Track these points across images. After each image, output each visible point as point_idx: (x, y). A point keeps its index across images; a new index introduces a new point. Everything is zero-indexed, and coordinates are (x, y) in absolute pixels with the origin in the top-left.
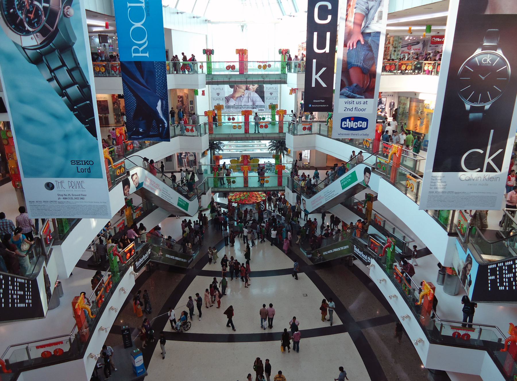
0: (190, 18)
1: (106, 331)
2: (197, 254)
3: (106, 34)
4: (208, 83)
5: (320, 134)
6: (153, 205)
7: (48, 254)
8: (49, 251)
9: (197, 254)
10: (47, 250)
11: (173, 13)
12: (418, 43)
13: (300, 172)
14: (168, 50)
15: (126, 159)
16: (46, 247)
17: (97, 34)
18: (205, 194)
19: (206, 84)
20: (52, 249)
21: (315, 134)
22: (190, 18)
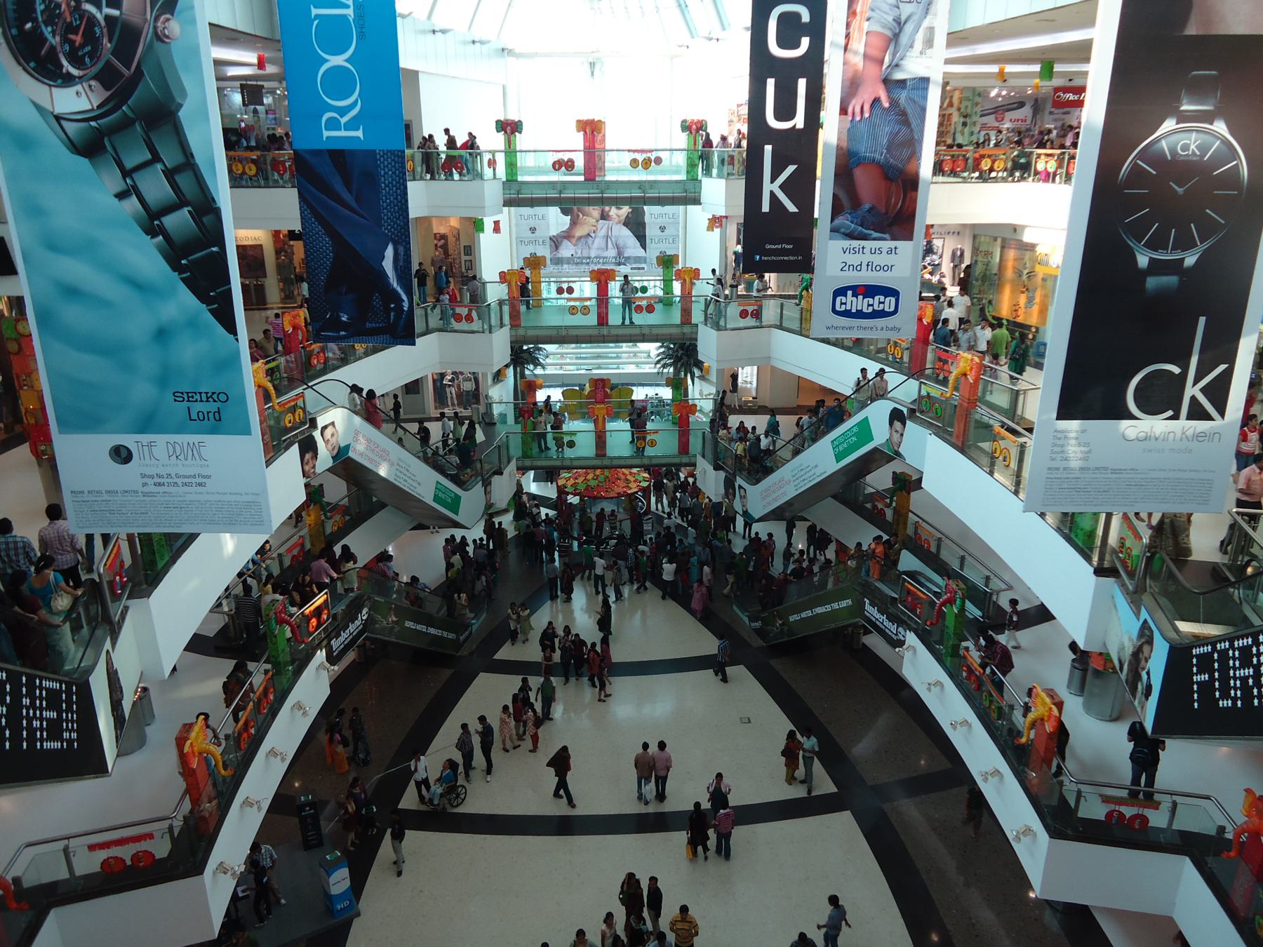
0: (465, 43)
1: (259, 809)
2: (481, 621)
3: (259, 83)
4: (508, 203)
5: (781, 327)
6: (374, 499)
7: (117, 619)
8: (119, 612)
9: (481, 621)
10: (115, 610)
11: (424, 32)
12: (1021, 105)
13: (734, 421)
14: (411, 121)
15: (309, 387)
16: (112, 602)
17: (238, 84)
18: (501, 474)
19: (504, 206)
20: (126, 608)
21: (770, 326)
22: (465, 43)
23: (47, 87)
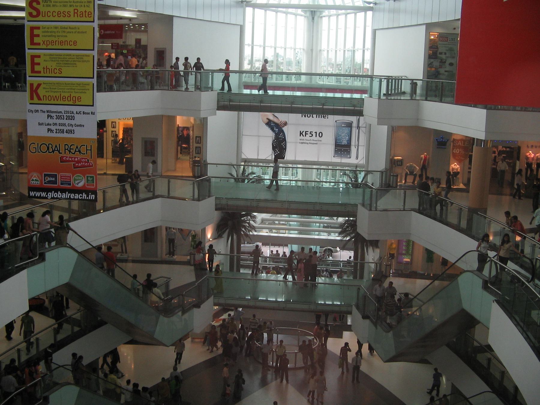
6: (99, 318)
23: (274, 13)
